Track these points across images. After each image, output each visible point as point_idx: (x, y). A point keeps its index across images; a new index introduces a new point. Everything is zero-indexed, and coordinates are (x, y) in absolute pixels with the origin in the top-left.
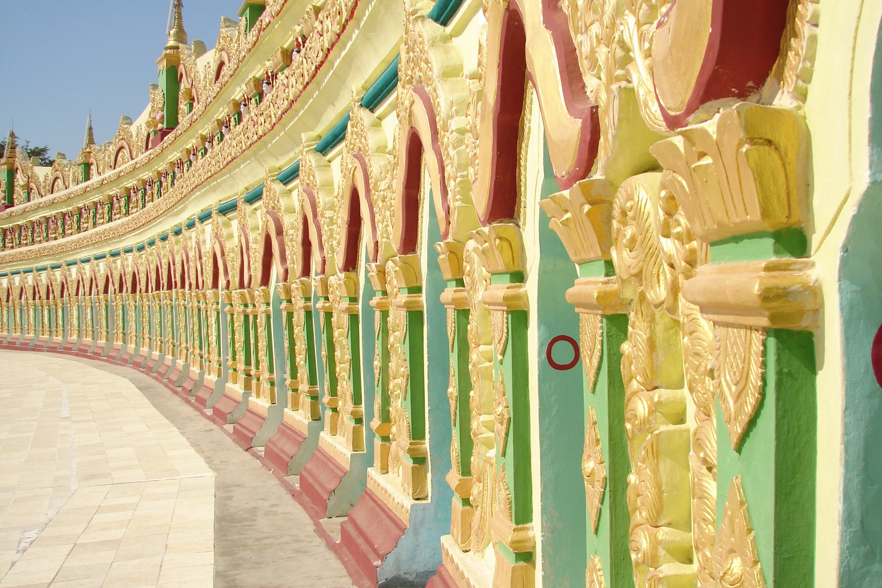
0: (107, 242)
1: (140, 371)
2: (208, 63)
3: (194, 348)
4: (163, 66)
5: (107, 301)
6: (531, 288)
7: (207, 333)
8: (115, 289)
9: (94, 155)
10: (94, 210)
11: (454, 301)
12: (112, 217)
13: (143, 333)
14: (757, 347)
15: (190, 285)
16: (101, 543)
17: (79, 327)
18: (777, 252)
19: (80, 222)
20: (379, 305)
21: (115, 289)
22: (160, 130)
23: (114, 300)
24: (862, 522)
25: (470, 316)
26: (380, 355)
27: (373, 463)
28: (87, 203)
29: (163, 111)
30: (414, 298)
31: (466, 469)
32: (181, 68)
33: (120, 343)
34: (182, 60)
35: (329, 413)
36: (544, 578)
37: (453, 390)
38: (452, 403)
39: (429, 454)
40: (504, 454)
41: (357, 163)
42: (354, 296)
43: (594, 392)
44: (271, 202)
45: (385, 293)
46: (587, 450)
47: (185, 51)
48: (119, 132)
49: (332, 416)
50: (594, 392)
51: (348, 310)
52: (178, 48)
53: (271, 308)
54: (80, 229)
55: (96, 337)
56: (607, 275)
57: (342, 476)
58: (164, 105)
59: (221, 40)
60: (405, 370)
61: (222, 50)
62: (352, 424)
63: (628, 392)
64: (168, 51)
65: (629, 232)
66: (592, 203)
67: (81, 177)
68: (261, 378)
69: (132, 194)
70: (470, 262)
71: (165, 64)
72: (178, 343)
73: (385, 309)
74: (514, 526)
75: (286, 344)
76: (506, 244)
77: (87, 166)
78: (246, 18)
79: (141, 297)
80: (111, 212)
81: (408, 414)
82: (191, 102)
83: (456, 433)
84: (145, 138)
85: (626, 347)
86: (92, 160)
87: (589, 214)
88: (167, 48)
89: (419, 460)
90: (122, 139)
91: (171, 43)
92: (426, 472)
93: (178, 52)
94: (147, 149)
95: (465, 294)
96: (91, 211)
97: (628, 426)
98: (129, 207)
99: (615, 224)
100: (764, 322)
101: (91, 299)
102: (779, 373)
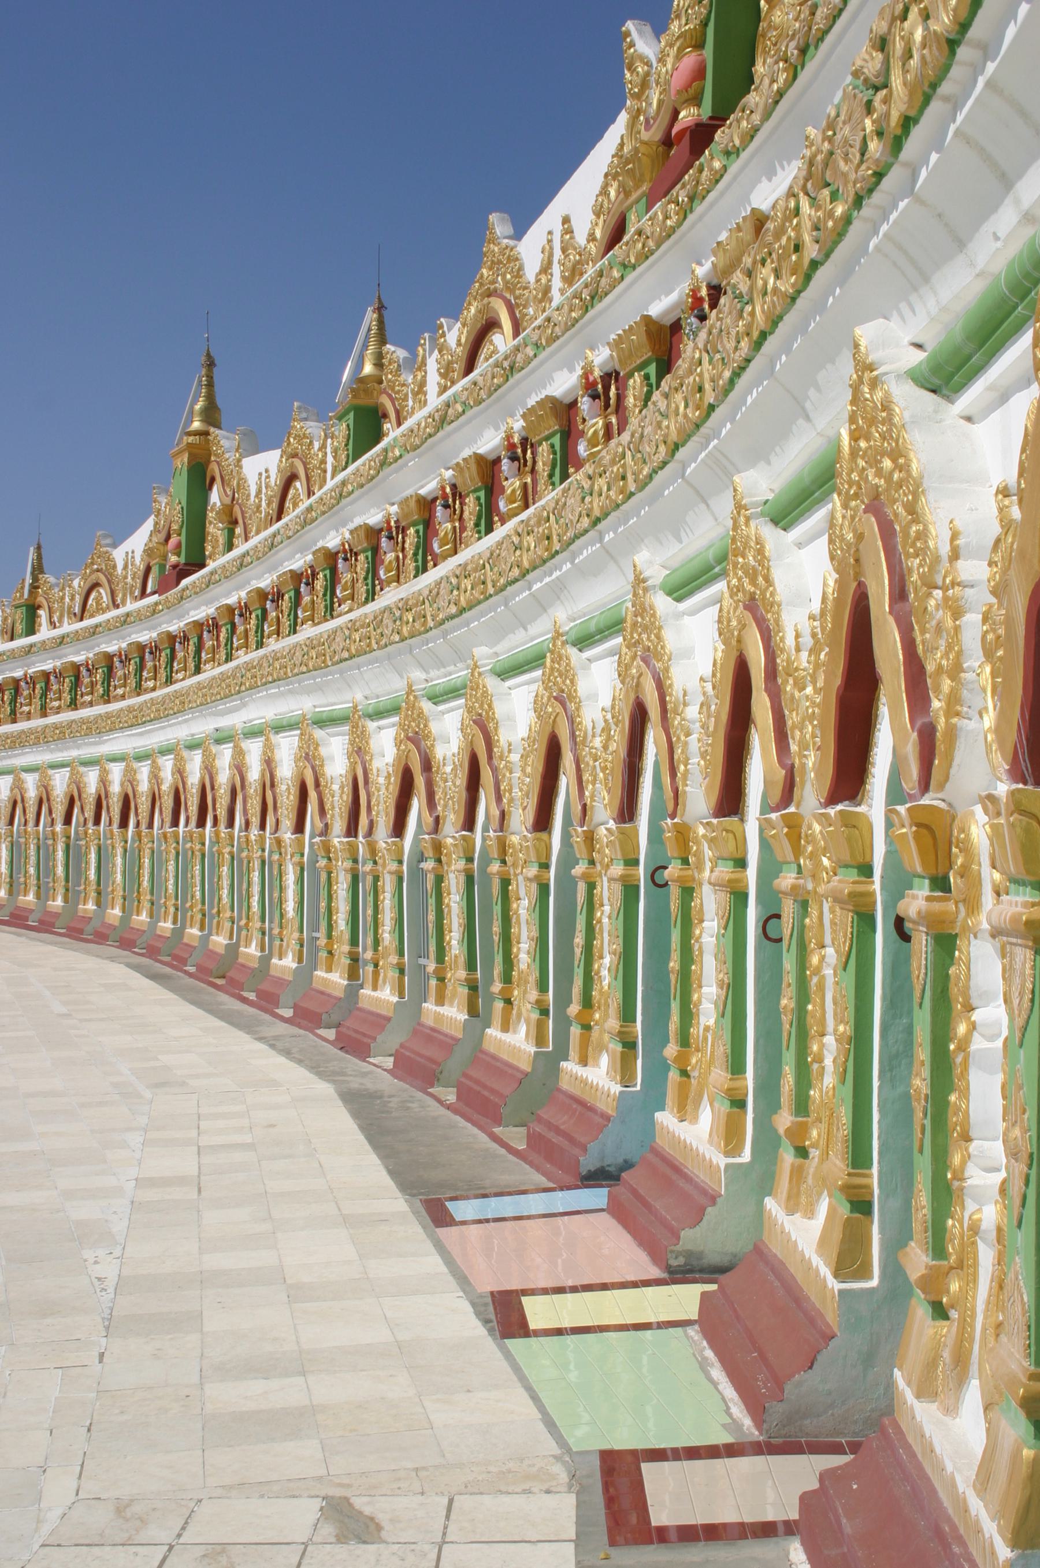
0: (74, 742)
1: (134, 953)
2: (267, 471)
3: (248, 918)
4: (182, 462)
5: (69, 837)
6: (751, 873)
7: (280, 897)
8: (85, 819)
9: (45, 593)
10: (43, 684)
11: (680, 880)
12: (76, 699)
13: (139, 892)
14: (850, 919)
15: (215, 819)
16: (222, 1146)
17: (11, 877)
18: (858, 875)
19: (16, 702)
20: (585, 876)
21: (85, 819)
22: (175, 567)
23: (83, 836)
24: (891, 1001)
25: (957, 953)
26: (584, 931)
27: (568, 1055)
28: (30, 671)
29: (179, 535)
30: (631, 871)
31: (685, 1040)
32: (214, 468)
33: (91, 906)
34: (215, 455)
35: (499, 1005)
36: (754, 1119)
37: (674, 964)
38: (673, 978)
39: (640, 1037)
40: (723, 1016)
41: (559, 708)
42: (543, 861)
43: (788, 951)
44: (413, 724)
45: (592, 862)
46: (784, 992)
47: (225, 441)
48: (92, 558)
49: (504, 1009)
50: (788, 951)
51: (537, 878)
52: (207, 433)
53: (405, 868)
54: (15, 715)
55: (43, 895)
56: (798, 873)
57: (521, 1079)
58: (182, 527)
59: (292, 440)
60: (618, 946)
61: (295, 455)
62: (535, 1015)
63: (809, 950)
64: (191, 439)
65: (810, 849)
66: (789, 827)
67: (19, 627)
68: (381, 963)
69: (117, 663)
70: (697, 843)
71: (186, 460)
72: (215, 911)
73: (592, 880)
74: (729, 1076)
75: (432, 917)
76: (731, 836)
77: (32, 610)
78: (348, 426)
79: (138, 835)
80: (76, 691)
81: (619, 995)
82: (231, 526)
83: (675, 1006)
84: (141, 574)
85: (807, 921)
86: (41, 600)
87: (786, 834)
88: (189, 434)
89: (629, 1045)
90: (98, 570)
91: (196, 425)
92: (636, 1058)
93: (207, 441)
94: (143, 594)
95: (690, 872)
96: (38, 686)
97: (808, 973)
98: (109, 685)
99: (803, 842)
100: (851, 908)
101: (38, 832)
102: (858, 931)
